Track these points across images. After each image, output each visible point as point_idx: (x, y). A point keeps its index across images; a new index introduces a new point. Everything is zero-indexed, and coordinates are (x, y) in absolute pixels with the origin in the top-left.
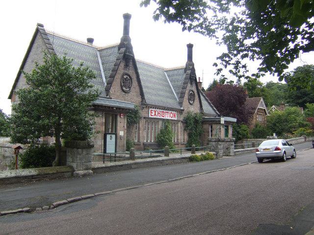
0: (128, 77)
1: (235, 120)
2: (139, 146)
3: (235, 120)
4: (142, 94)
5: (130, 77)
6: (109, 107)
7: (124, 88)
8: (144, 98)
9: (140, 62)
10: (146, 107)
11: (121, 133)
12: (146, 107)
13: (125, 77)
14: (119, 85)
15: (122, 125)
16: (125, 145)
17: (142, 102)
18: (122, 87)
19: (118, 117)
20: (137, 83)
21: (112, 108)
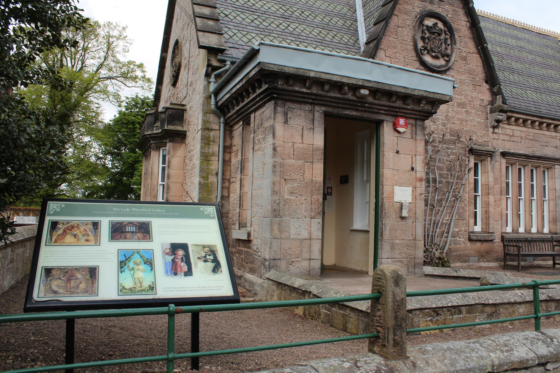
0: (440, 25)
1: (175, 370)
2: (486, 245)
3: (175, 370)
4: (491, 79)
5: (445, 23)
6: (338, 86)
7: (428, 59)
8: (500, 92)
9: (487, 18)
10: (509, 118)
11: (402, 194)
12: (509, 118)
13: (429, 22)
14: (411, 47)
15: (404, 162)
16: (421, 244)
17: (492, 103)
18: (419, 54)
19: (387, 130)
20: (471, 46)
21: (355, 88)
